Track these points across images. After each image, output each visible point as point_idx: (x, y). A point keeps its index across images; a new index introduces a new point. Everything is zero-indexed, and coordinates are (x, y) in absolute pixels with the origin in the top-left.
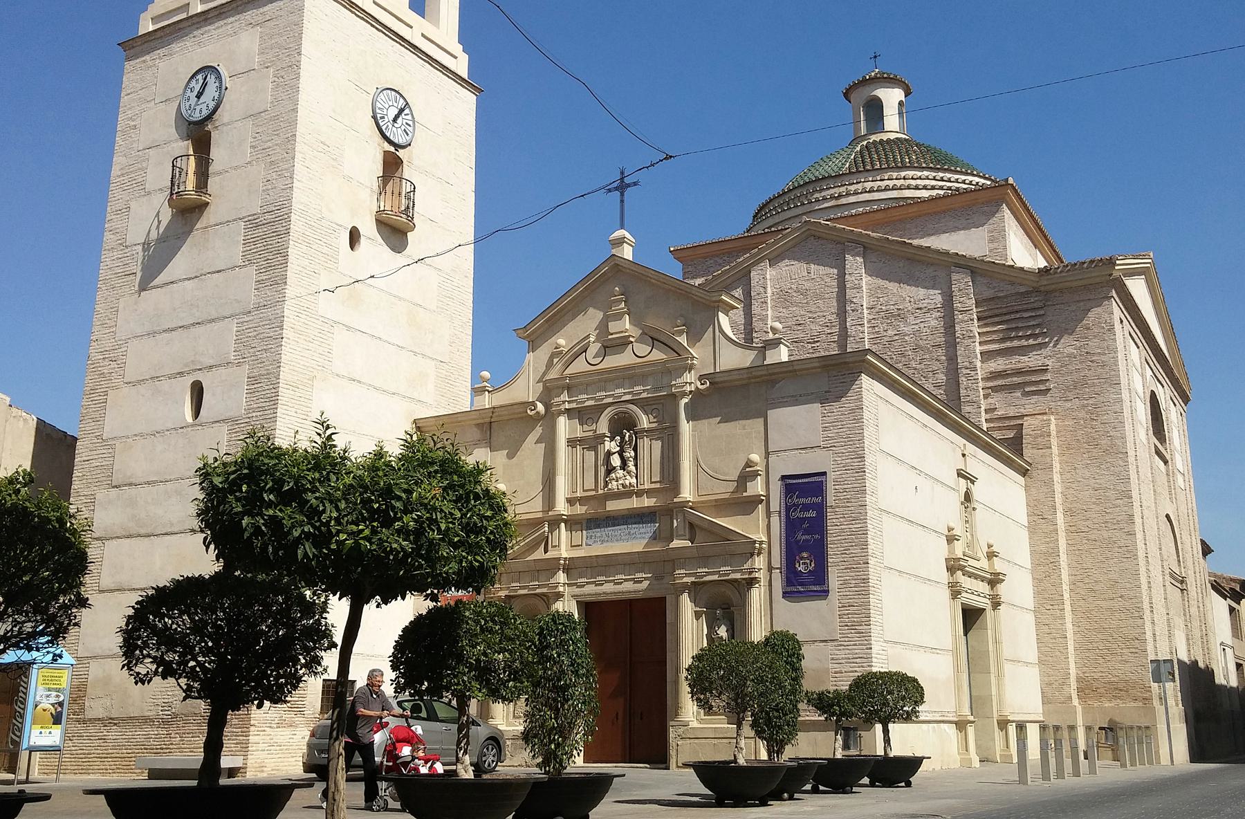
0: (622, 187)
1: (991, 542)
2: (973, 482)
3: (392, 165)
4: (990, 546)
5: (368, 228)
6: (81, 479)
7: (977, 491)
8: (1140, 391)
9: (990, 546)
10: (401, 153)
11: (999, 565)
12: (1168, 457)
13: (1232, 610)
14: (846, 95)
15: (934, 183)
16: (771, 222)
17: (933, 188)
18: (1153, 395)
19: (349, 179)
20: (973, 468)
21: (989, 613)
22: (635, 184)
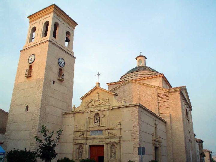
0: (98, 75)
1: (160, 135)
2: (146, 58)
3: (61, 70)
4: (159, 136)
5: (56, 80)
6: (149, 105)
7: (158, 127)
8: (184, 109)
9: (159, 136)
10: (62, 68)
11: (160, 140)
12: (189, 120)
13: (199, 145)
14: (136, 59)
15: (150, 74)
16: (123, 79)
17: (150, 74)
18: (186, 109)
19: (54, 73)
20: (157, 123)
21: (159, 148)
22: (101, 74)
